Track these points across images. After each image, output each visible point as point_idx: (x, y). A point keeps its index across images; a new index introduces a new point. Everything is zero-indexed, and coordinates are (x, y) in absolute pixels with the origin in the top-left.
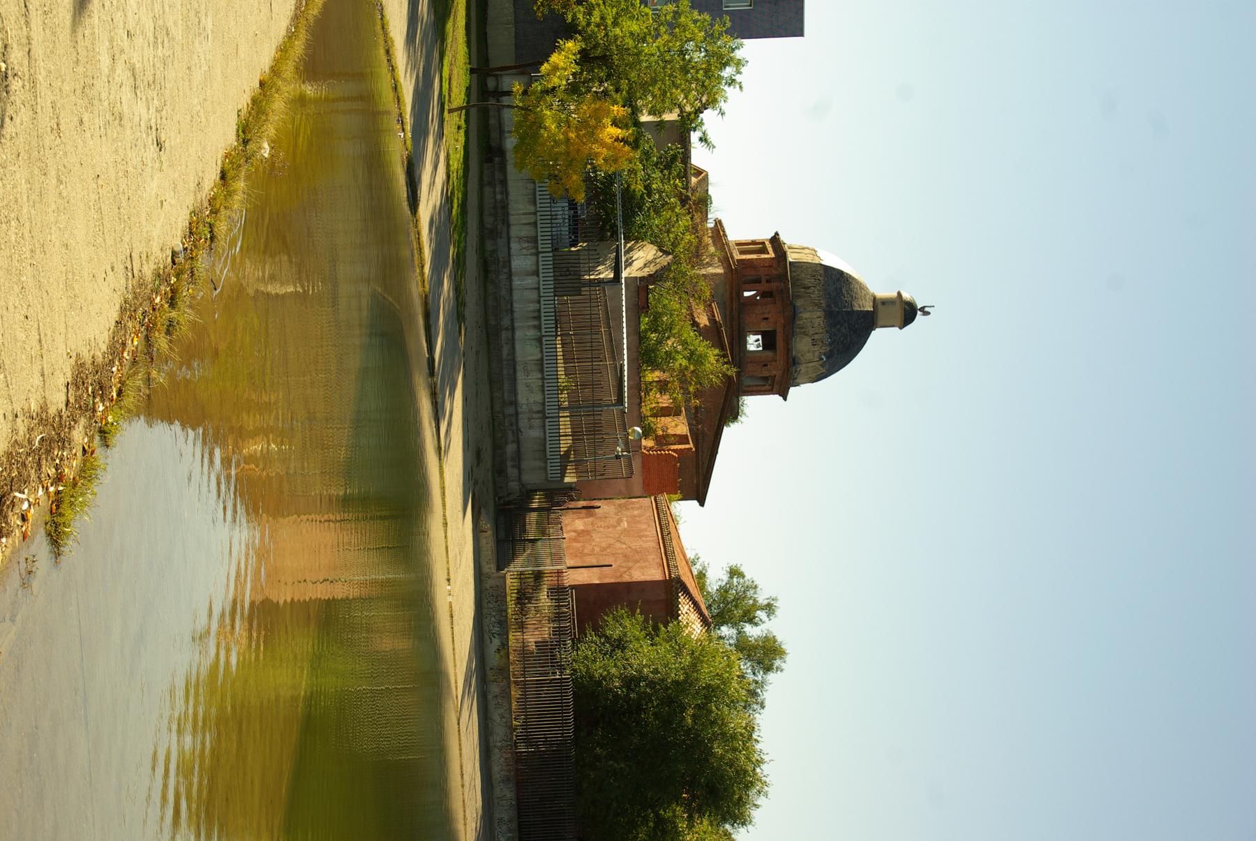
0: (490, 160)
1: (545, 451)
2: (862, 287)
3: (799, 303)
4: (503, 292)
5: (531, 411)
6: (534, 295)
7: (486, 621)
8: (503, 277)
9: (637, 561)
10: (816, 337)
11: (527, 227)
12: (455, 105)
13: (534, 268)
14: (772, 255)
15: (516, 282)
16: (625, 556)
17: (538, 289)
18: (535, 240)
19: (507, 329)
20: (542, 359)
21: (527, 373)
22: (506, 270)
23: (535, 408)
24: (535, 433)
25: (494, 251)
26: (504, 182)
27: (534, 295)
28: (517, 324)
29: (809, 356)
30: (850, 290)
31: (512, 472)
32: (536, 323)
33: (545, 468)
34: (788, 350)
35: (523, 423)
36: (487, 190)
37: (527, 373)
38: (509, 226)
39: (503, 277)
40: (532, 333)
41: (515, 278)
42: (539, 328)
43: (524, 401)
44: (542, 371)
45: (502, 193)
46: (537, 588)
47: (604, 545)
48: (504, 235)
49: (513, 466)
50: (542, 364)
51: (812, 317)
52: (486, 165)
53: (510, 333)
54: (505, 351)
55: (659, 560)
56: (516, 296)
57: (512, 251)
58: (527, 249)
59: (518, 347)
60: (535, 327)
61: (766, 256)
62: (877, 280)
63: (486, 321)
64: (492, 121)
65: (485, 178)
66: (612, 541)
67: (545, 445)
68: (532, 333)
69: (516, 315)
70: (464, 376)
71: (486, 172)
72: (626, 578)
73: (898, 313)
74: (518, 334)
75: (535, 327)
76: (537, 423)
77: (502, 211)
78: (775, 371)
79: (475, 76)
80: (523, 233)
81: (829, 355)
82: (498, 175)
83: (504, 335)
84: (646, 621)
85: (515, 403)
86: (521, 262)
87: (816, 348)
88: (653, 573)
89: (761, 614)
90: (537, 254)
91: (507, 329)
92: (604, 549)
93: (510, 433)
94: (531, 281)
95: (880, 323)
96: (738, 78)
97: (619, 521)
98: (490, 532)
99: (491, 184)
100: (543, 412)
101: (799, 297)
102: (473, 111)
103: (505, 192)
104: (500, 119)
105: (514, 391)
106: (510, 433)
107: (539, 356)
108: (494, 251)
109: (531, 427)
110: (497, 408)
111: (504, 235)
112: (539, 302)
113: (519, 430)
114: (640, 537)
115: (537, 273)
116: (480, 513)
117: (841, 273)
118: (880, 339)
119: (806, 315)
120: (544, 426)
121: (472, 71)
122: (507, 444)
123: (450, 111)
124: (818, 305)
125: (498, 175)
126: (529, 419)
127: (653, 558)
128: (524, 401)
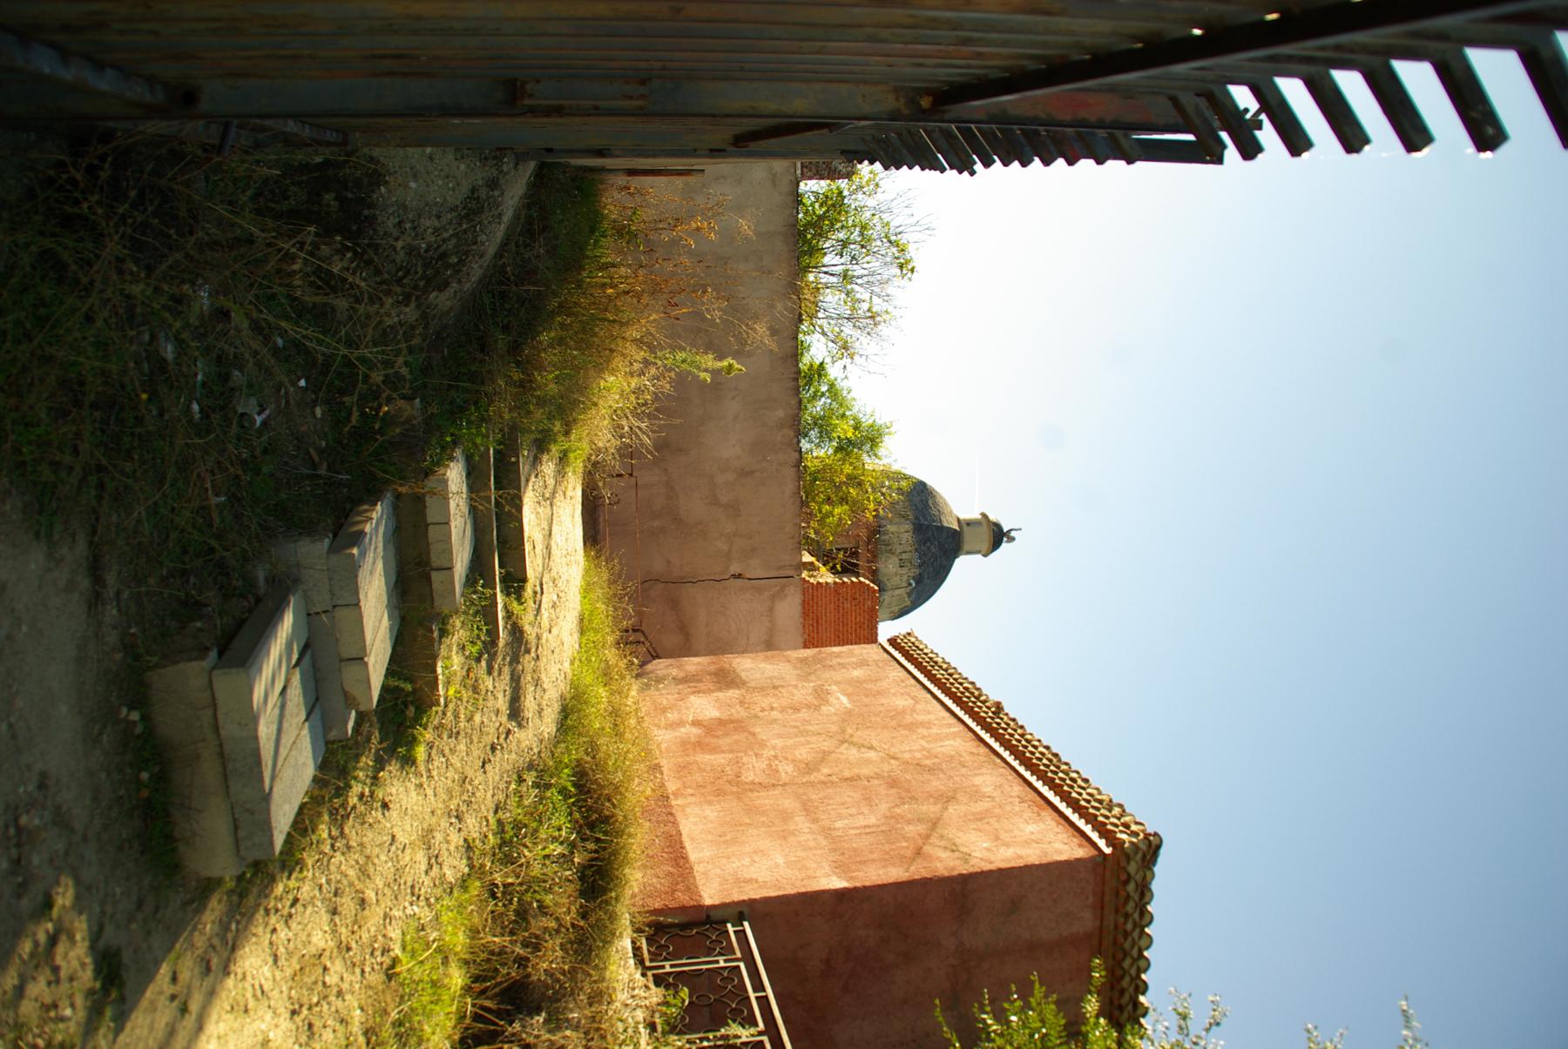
9: (948, 799)
10: (904, 556)
16: (893, 783)
29: (896, 581)
30: (935, 503)
46: (587, 944)
47: (803, 753)
55: (1017, 788)
62: (961, 502)
66: (826, 745)
72: (943, 863)
73: (986, 537)
87: (904, 571)
92: (809, 768)
95: (966, 547)
97: (821, 695)
114: (911, 727)
118: (963, 565)
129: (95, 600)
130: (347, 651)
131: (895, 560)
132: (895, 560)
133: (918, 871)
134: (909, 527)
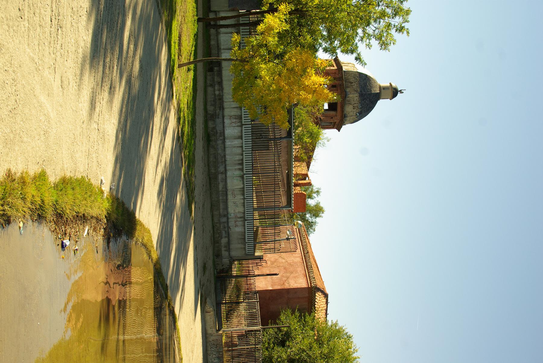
0: (211, 70)
1: (245, 239)
2: (375, 82)
3: (348, 90)
4: (220, 151)
5: (236, 217)
6: (239, 151)
7: (210, 357)
8: (220, 142)
9: (292, 273)
10: (355, 105)
11: (236, 110)
12: (184, 60)
13: (239, 134)
14: (336, 68)
15: (228, 143)
16: (285, 268)
17: (242, 147)
18: (240, 117)
19: (222, 173)
20: (243, 188)
21: (234, 196)
22: (221, 138)
23: (239, 215)
24: (239, 229)
25: (214, 128)
26: (220, 83)
27: (239, 151)
28: (228, 168)
29: (351, 114)
30: (370, 84)
31: (224, 253)
32: (240, 167)
33: (245, 248)
34: (343, 111)
35: (232, 223)
36: (210, 89)
37: (234, 196)
38: (223, 109)
39: (220, 142)
40: (238, 173)
41: (227, 141)
42: (242, 170)
43: (232, 212)
44: (243, 195)
45: (219, 90)
48: (221, 116)
49: (225, 250)
50: (244, 191)
51: (354, 97)
52: (208, 73)
53: (224, 176)
54: (221, 186)
55: (303, 272)
56: (228, 151)
57: (225, 124)
58: (235, 123)
59: (229, 181)
60: (239, 169)
61: (333, 68)
63: (209, 170)
64: (213, 42)
65: (208, 82)
67: (245, 236)
68: (238, 173)
69: (227, 163)
70: (195, 234)
71: (209, 78)
72: (287, 286)
73: (390, 93)
74: (229, 174)
75: (239, 169)
76: (240, 223)
77: (219, 101)
78: (337, 120)
79: (201, 23)
80: (233, 114)
81: (360, 113)
82: (216, 79)
83: (220, 177)
84: (300, 316)
85: (226, 215)
86: (231, 130)
87: (355, 110)
88: (299, 282)
89: (315, 195)
90: (242, 126)
91: (222, 173)
93: (224, 232)
94: (237, 142)
95: (382, 96)
96: (406, 25)
98: (212, 313)
99: (212, 85)
100: (244, 217)
101: (348, 87)
102: (200, 66)
103: (221, 89)
104: (218, 41)
105: (226, 208)
106: (224, 232)
107: (242, 186)
108: (214, 128)
109: (236, 226)
110: (216, 220)
111: (221, 116)
112: (242, 155)
113: (229, 227)
115: (241, 137)
116: (206, 303)
117: (366, 76)
118: (381, 104)
119: (351, 96)
120: (244, 225)
121: (199, 20)
122: (222, 238)
123: (180, 66)
124: (356, 91)
125: (216, 79)
126: (235, 222)
127: (300, 270)
128: (232, 212)
129: (69, 321)
130: (201, 24)
131: (351, 107)
132: (351, 107)
133: (282, 287)
134: (357, 95)
